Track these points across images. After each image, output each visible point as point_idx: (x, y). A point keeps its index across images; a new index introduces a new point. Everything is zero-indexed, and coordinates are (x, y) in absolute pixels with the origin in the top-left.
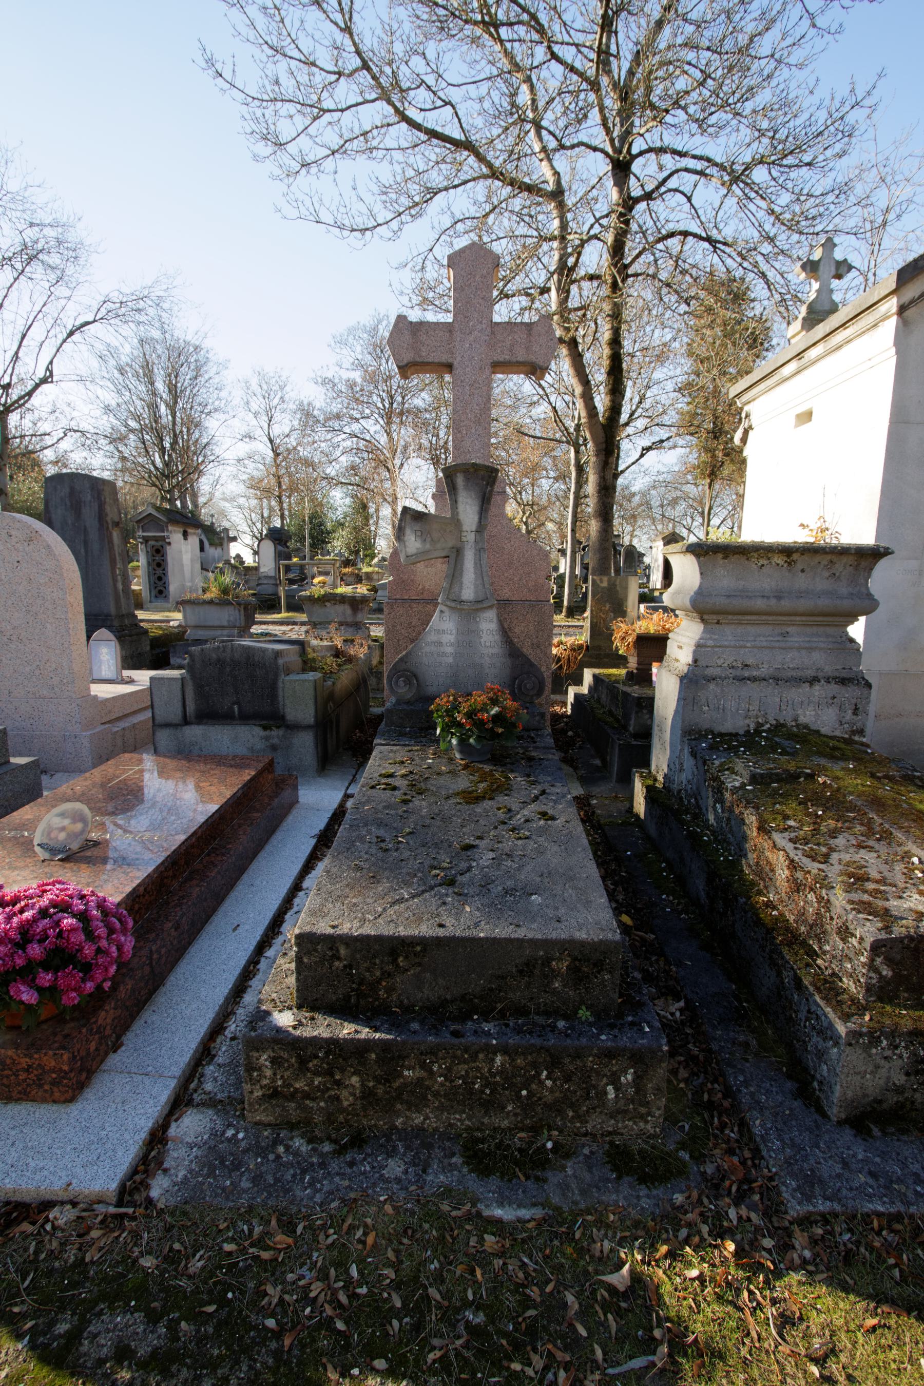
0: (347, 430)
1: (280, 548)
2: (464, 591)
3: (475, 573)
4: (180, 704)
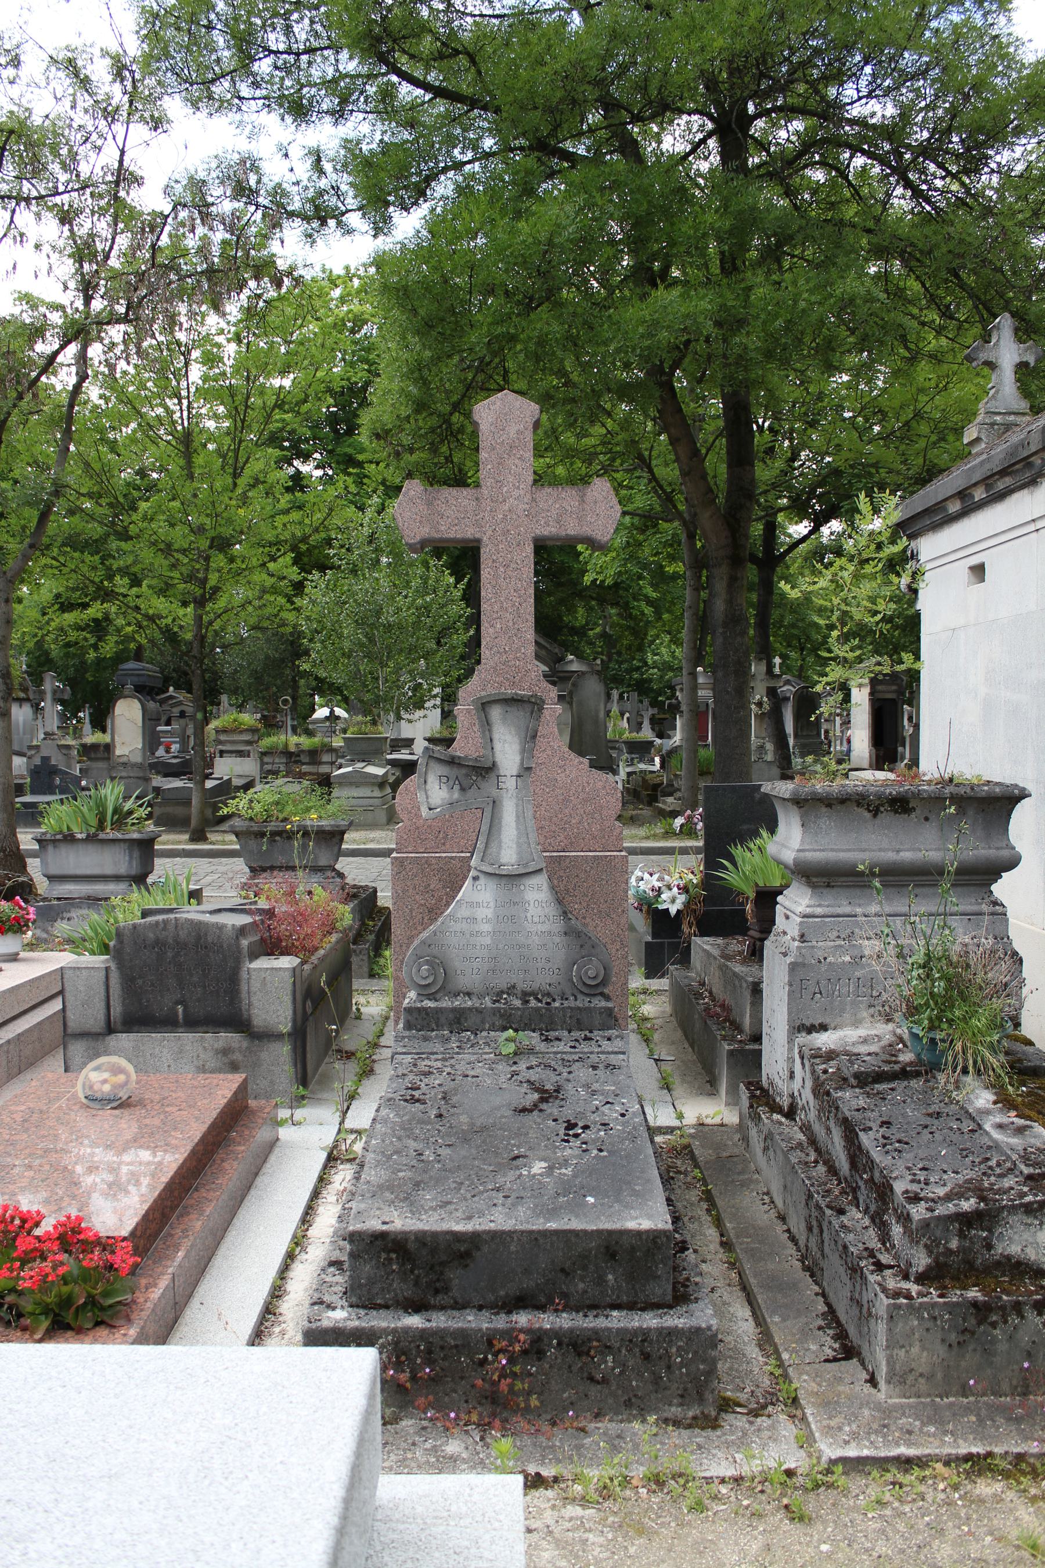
0: (84, 225)
1: (152, 705)
2: (503, 852)
3: (518, 829)
4: (103, 1004)
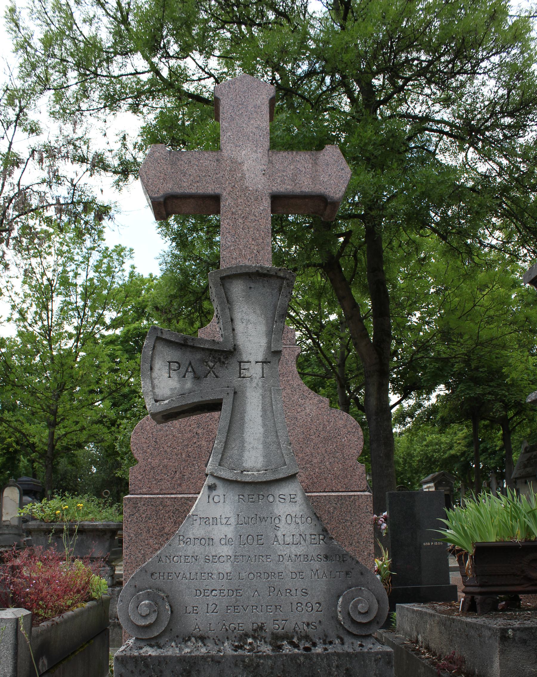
2: (246, 454)
3: (264, 425)
